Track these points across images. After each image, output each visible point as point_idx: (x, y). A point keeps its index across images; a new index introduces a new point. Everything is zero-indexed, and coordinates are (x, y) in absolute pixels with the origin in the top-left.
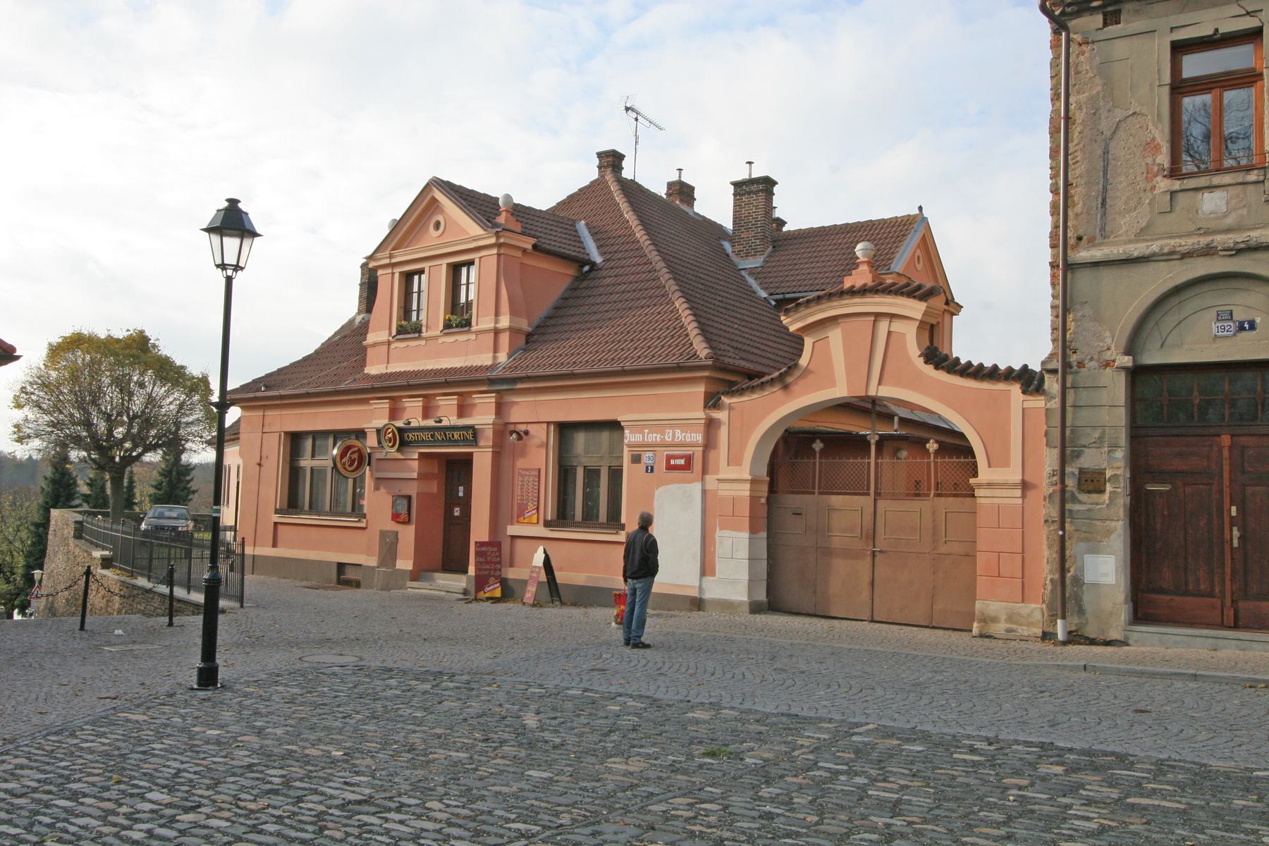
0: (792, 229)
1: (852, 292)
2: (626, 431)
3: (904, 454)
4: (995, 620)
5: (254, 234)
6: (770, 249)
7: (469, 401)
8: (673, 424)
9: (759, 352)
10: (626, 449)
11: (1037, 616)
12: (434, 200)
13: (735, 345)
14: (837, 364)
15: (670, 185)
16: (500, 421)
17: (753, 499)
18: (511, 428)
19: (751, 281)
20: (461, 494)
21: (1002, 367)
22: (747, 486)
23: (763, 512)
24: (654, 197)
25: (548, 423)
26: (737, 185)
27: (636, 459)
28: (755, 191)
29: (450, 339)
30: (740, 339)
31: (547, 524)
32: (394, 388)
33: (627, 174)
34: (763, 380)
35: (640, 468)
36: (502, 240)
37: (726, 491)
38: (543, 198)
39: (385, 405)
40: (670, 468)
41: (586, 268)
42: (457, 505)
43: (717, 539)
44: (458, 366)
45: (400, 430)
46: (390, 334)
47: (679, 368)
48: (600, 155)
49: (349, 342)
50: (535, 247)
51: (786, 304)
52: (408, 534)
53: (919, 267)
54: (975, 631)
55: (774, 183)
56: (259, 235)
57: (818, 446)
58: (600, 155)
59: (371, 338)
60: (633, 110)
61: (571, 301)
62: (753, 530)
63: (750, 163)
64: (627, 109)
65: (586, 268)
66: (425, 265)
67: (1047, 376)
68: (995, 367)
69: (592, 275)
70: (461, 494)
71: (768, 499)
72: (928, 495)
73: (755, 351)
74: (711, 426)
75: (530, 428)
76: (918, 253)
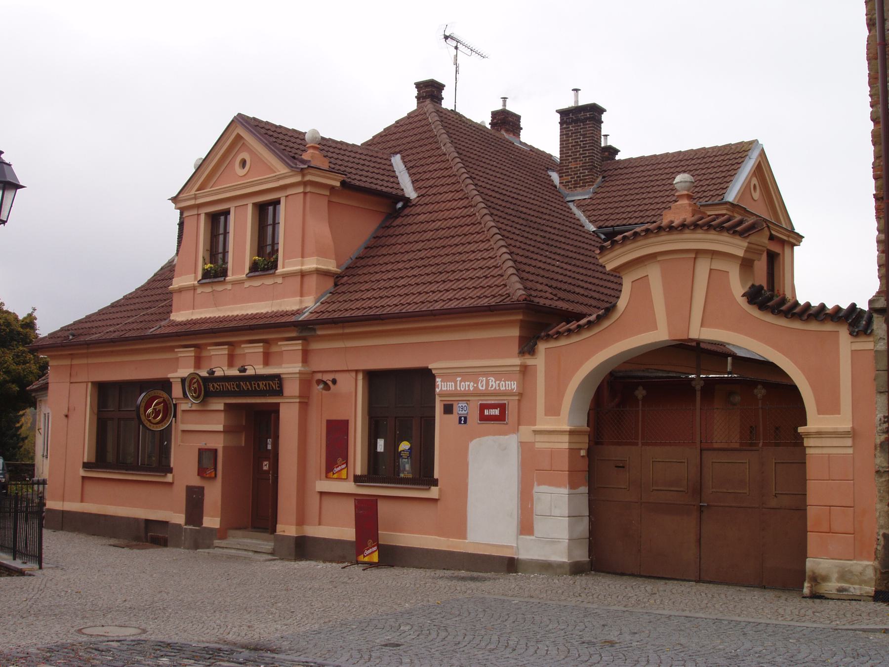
0: (622, 158)
1: (670, 228)
2: (438, 380)
3: (737, 399)
4: (826, 579)
5: (17, 186)
6: (600, 179)
7: (238, 351)
8: (487, 372)
9: (582, 291)
10: (438, 399)
11: (870, 574)
12: (239, 137)
13: (554, 284)
14: (667, 303)
15: (495, 114)
16: (307, 369)
17: (573, 451)
18: (319, 376)
19: (579, 214)
20: (269, 447)
21: (830, 306)
22: (566, 438)
23: (584, 465)
24: (478, 128)
25: (357, 371)
26: (564, 113)
27: (448, 409)
28: (581, 120)
29: (257, 283)
30: (560, 278)
31: (357, 479)
32: (198, 335)
33: (447, 103)
34: (583, 321)
35: (454, 418)
36: (308, 178)
37: (542, 443)
38: (357, 129)
39: (190, 353)
40: (483, 418)
41: (400, 205)
42: (266, 459)
43: (535, 496)
44: (264, 311)
45: (204, 379)
46: (196, 278)
47: (490, 310)
48: (419, 85)
49: (159, 289)
50: (343, 183)
51: (612, 237)
52: (213, 494)
53: (756, 195)
54: (806, 591)
55: (602, 111)
56: (22, 187)
57: (640, 393)
58: (419, 85)
59: (177, 283)
60: (452, 38)
61: (383, 240)
62: (573, 485)
63: (576, 90)
64: (446, 37)
65: (400, 205)
66: (231, 206)
67: (875, 315)
68: (823, 307)
69: (406, 211)
70: (269, 447)
71: (589, 451)
72: (756, 445)
73: (577, 290)
74: (524, 370)
75: (338, 377)
76: (754, 181)
